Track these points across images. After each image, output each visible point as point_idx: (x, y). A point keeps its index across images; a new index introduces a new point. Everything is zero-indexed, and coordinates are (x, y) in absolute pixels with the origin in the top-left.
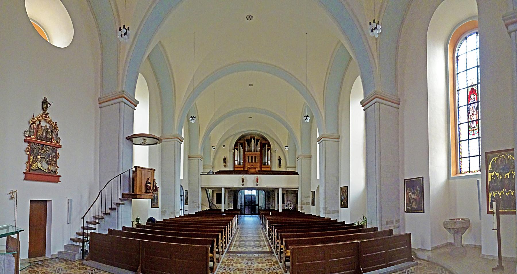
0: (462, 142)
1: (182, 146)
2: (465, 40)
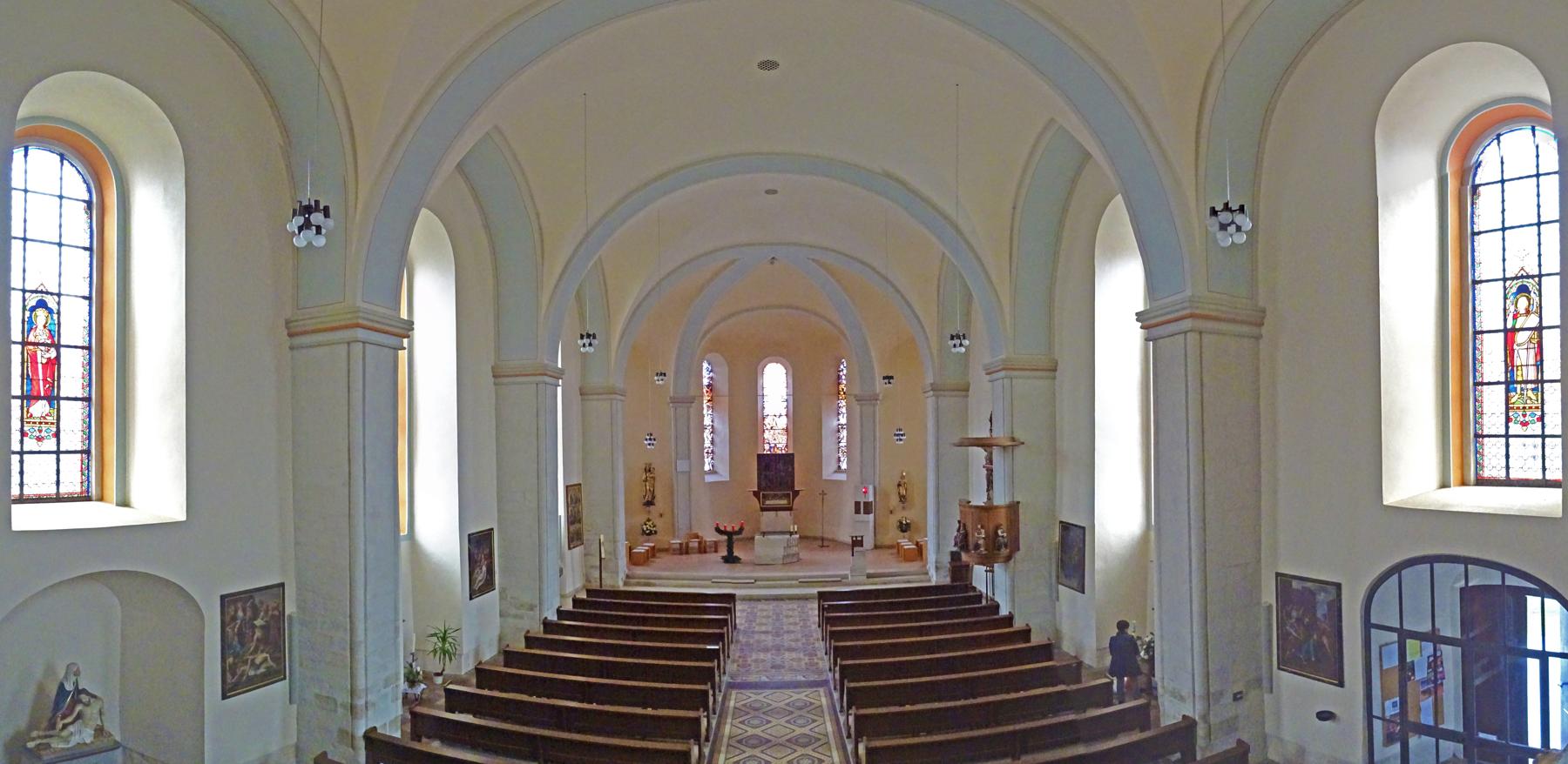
0: (1484, 284)
1: (559, 389)
2: (1496, 141)
